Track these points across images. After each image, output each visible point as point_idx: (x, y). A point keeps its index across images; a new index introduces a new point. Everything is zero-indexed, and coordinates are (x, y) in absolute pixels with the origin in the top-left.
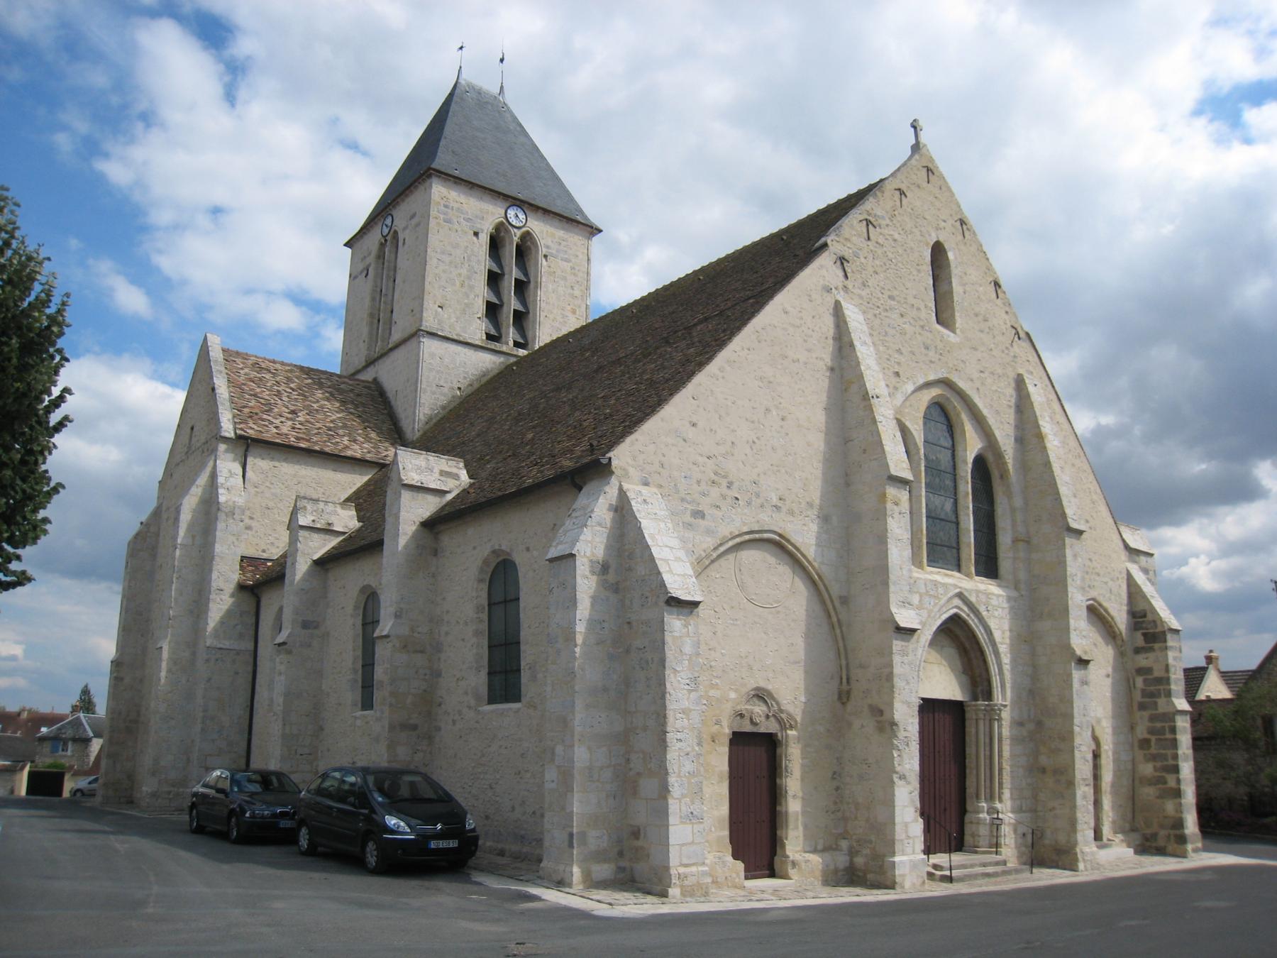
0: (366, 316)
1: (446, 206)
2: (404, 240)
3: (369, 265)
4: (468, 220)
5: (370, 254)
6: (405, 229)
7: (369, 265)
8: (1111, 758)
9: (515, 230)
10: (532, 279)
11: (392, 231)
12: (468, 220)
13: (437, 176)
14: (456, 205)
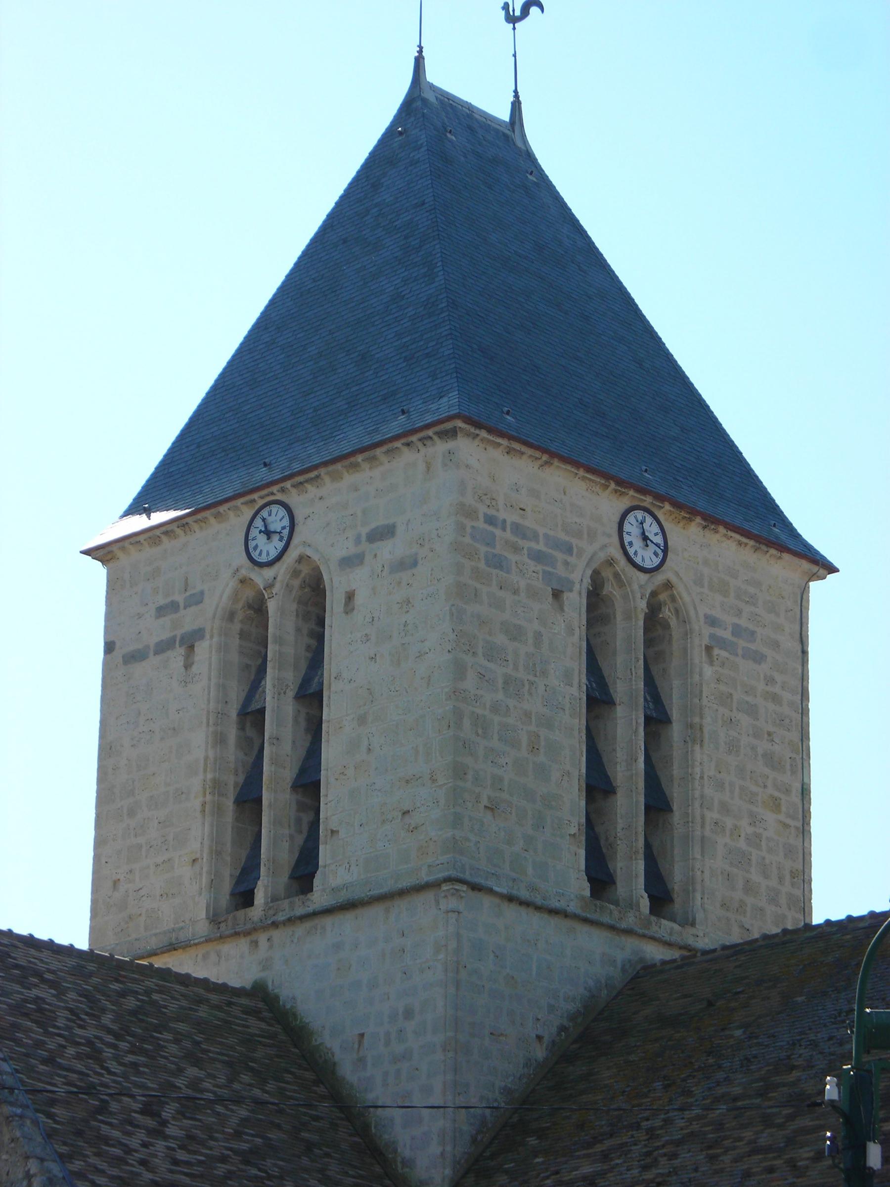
0: (196, 783)
1: (491, 520)
2: (350, 597)
3: (199, 634)
4: (538, 557)
5: (197, 599)
6: (349, 562)
7: (199, 634)
8: (242, 865)
9: (643, 577)
10: (675, 715)
11: (292, 555)
12: (538, 557)
13: (468, 435)
14: (512, 517)
